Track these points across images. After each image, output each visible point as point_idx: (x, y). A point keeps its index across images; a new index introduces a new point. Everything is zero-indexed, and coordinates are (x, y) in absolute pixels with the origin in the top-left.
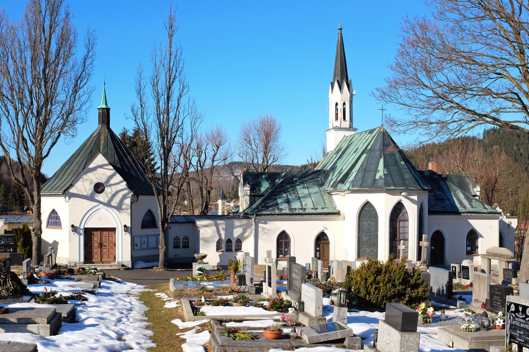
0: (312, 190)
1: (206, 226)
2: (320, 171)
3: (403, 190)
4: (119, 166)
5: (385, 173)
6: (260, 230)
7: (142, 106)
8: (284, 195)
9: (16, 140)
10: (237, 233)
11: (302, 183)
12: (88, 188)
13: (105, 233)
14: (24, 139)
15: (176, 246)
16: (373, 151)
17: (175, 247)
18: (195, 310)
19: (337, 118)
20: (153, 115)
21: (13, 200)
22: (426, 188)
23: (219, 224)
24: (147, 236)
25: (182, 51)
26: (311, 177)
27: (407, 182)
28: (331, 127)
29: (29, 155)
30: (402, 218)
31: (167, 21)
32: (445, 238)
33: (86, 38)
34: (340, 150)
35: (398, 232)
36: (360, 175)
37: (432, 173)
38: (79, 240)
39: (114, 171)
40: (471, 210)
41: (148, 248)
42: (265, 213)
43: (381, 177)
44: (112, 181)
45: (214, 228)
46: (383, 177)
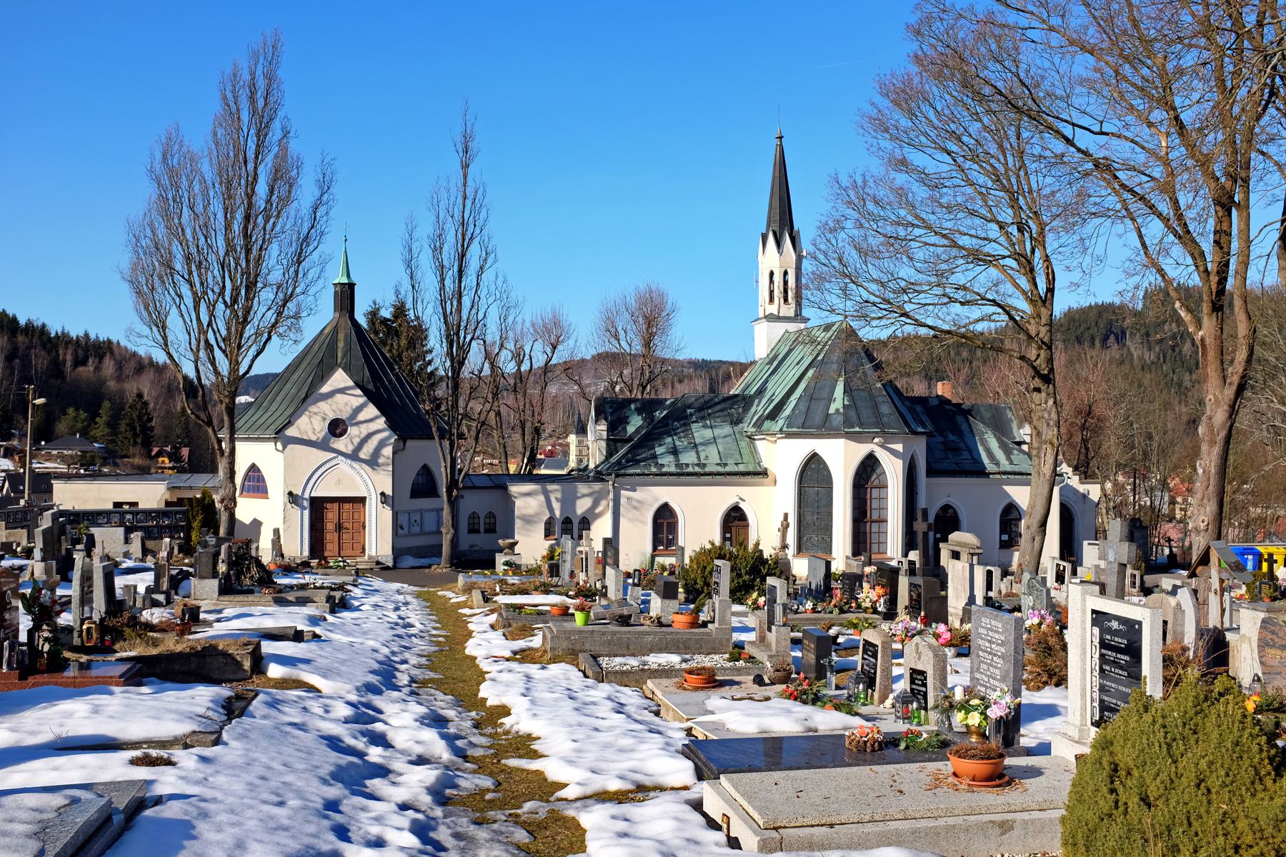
0: (717, 432)
1: (528, 494)
2: (736, 396)
3: (876, 435)
4: (371, 387)
5: (846, 403)
6: (623, 501)
7: (413, 287)
8: (669, 440)
9: (194, 347)
10: (582, 506)
11: (703, 418)
12: (318, 429)
13: (346, 506)
14: (209, 346)
15: (473, 530)
16: (827, 363)
17: (471, 531)
18: (486, 600)
19: (771, 300)
20: (432, 304)
21: (129, 435)
22: (920, 430)
23: (551, 492)
24: (421, 512)
25: (485, 191)
26: (719, 407)
27: (885, 420)
28: (761, 315)
29: (217, 372)
30: (876, 483)
31: (459, 139)
32: (961, 518)
33: (319, 171)
34: (775, 357)
35: (868, 508)
36: (803, 407)
37: (943, 401)
38: (302, 518)
39: (365, 398)
40: (1009, 468)
41: (422, 533)
42: (631, 471)
43: (837, 410)
44: (361, 417)
45: (542, 498)
46: (841, 410)
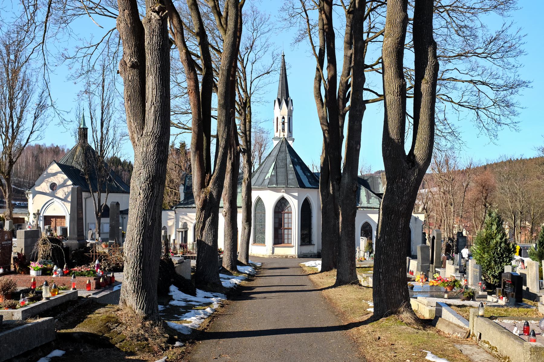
13: (58, 220)
27: (289, 181)
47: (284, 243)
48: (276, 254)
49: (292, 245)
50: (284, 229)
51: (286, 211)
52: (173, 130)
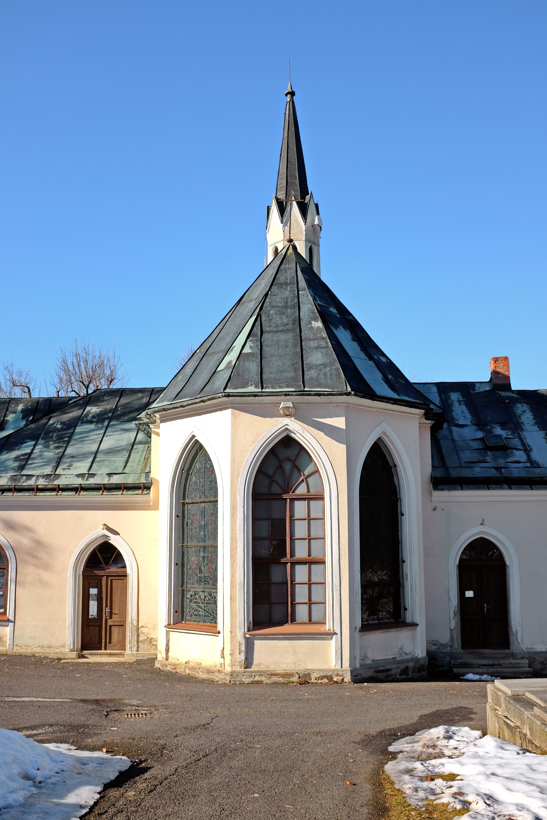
27: (310, 374)
47: (293, 620)
48: (263, 668)
49: (328, 627)
50: (293, 564)
51: (301, 490)
52: (143, 445)
